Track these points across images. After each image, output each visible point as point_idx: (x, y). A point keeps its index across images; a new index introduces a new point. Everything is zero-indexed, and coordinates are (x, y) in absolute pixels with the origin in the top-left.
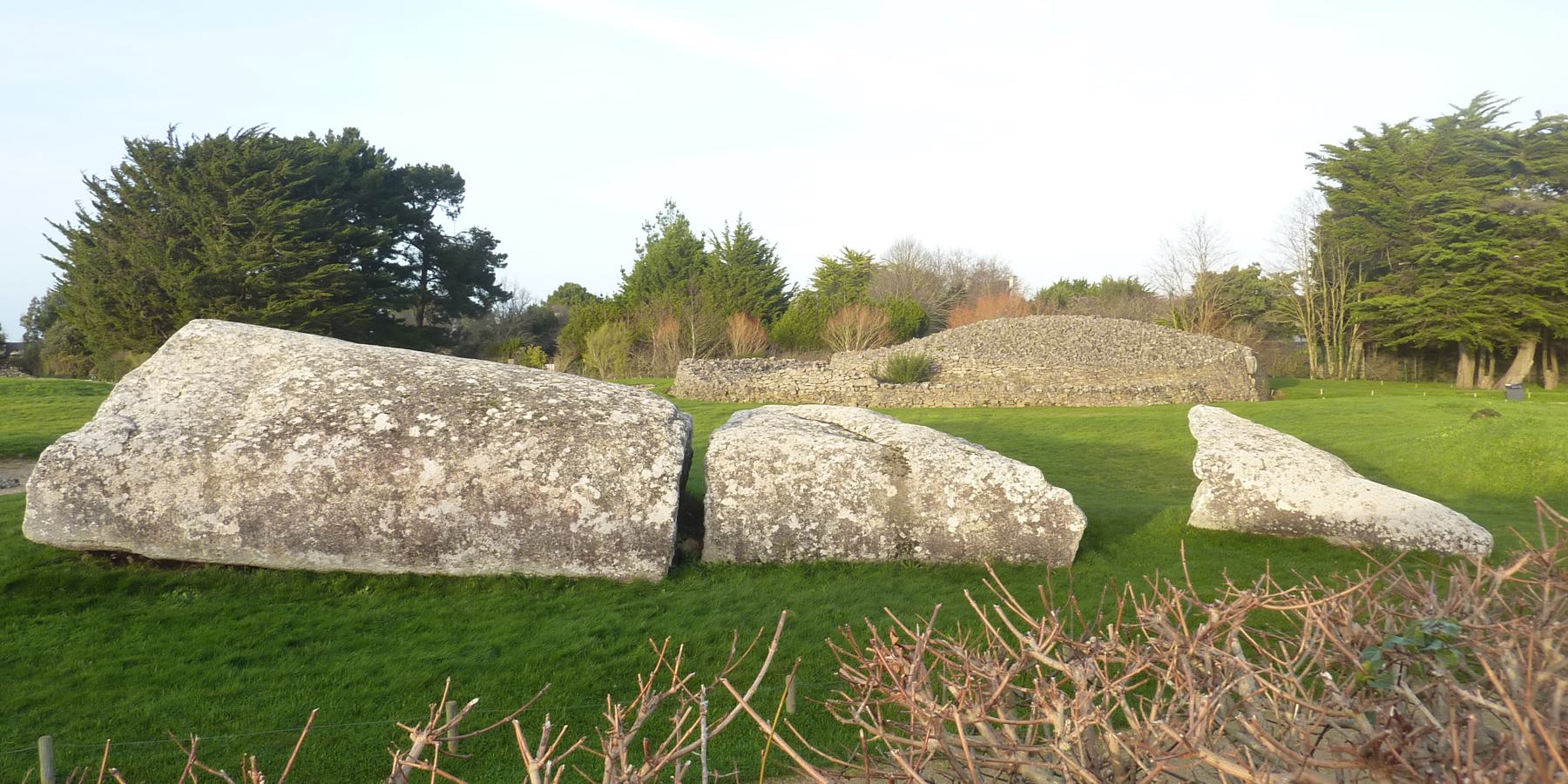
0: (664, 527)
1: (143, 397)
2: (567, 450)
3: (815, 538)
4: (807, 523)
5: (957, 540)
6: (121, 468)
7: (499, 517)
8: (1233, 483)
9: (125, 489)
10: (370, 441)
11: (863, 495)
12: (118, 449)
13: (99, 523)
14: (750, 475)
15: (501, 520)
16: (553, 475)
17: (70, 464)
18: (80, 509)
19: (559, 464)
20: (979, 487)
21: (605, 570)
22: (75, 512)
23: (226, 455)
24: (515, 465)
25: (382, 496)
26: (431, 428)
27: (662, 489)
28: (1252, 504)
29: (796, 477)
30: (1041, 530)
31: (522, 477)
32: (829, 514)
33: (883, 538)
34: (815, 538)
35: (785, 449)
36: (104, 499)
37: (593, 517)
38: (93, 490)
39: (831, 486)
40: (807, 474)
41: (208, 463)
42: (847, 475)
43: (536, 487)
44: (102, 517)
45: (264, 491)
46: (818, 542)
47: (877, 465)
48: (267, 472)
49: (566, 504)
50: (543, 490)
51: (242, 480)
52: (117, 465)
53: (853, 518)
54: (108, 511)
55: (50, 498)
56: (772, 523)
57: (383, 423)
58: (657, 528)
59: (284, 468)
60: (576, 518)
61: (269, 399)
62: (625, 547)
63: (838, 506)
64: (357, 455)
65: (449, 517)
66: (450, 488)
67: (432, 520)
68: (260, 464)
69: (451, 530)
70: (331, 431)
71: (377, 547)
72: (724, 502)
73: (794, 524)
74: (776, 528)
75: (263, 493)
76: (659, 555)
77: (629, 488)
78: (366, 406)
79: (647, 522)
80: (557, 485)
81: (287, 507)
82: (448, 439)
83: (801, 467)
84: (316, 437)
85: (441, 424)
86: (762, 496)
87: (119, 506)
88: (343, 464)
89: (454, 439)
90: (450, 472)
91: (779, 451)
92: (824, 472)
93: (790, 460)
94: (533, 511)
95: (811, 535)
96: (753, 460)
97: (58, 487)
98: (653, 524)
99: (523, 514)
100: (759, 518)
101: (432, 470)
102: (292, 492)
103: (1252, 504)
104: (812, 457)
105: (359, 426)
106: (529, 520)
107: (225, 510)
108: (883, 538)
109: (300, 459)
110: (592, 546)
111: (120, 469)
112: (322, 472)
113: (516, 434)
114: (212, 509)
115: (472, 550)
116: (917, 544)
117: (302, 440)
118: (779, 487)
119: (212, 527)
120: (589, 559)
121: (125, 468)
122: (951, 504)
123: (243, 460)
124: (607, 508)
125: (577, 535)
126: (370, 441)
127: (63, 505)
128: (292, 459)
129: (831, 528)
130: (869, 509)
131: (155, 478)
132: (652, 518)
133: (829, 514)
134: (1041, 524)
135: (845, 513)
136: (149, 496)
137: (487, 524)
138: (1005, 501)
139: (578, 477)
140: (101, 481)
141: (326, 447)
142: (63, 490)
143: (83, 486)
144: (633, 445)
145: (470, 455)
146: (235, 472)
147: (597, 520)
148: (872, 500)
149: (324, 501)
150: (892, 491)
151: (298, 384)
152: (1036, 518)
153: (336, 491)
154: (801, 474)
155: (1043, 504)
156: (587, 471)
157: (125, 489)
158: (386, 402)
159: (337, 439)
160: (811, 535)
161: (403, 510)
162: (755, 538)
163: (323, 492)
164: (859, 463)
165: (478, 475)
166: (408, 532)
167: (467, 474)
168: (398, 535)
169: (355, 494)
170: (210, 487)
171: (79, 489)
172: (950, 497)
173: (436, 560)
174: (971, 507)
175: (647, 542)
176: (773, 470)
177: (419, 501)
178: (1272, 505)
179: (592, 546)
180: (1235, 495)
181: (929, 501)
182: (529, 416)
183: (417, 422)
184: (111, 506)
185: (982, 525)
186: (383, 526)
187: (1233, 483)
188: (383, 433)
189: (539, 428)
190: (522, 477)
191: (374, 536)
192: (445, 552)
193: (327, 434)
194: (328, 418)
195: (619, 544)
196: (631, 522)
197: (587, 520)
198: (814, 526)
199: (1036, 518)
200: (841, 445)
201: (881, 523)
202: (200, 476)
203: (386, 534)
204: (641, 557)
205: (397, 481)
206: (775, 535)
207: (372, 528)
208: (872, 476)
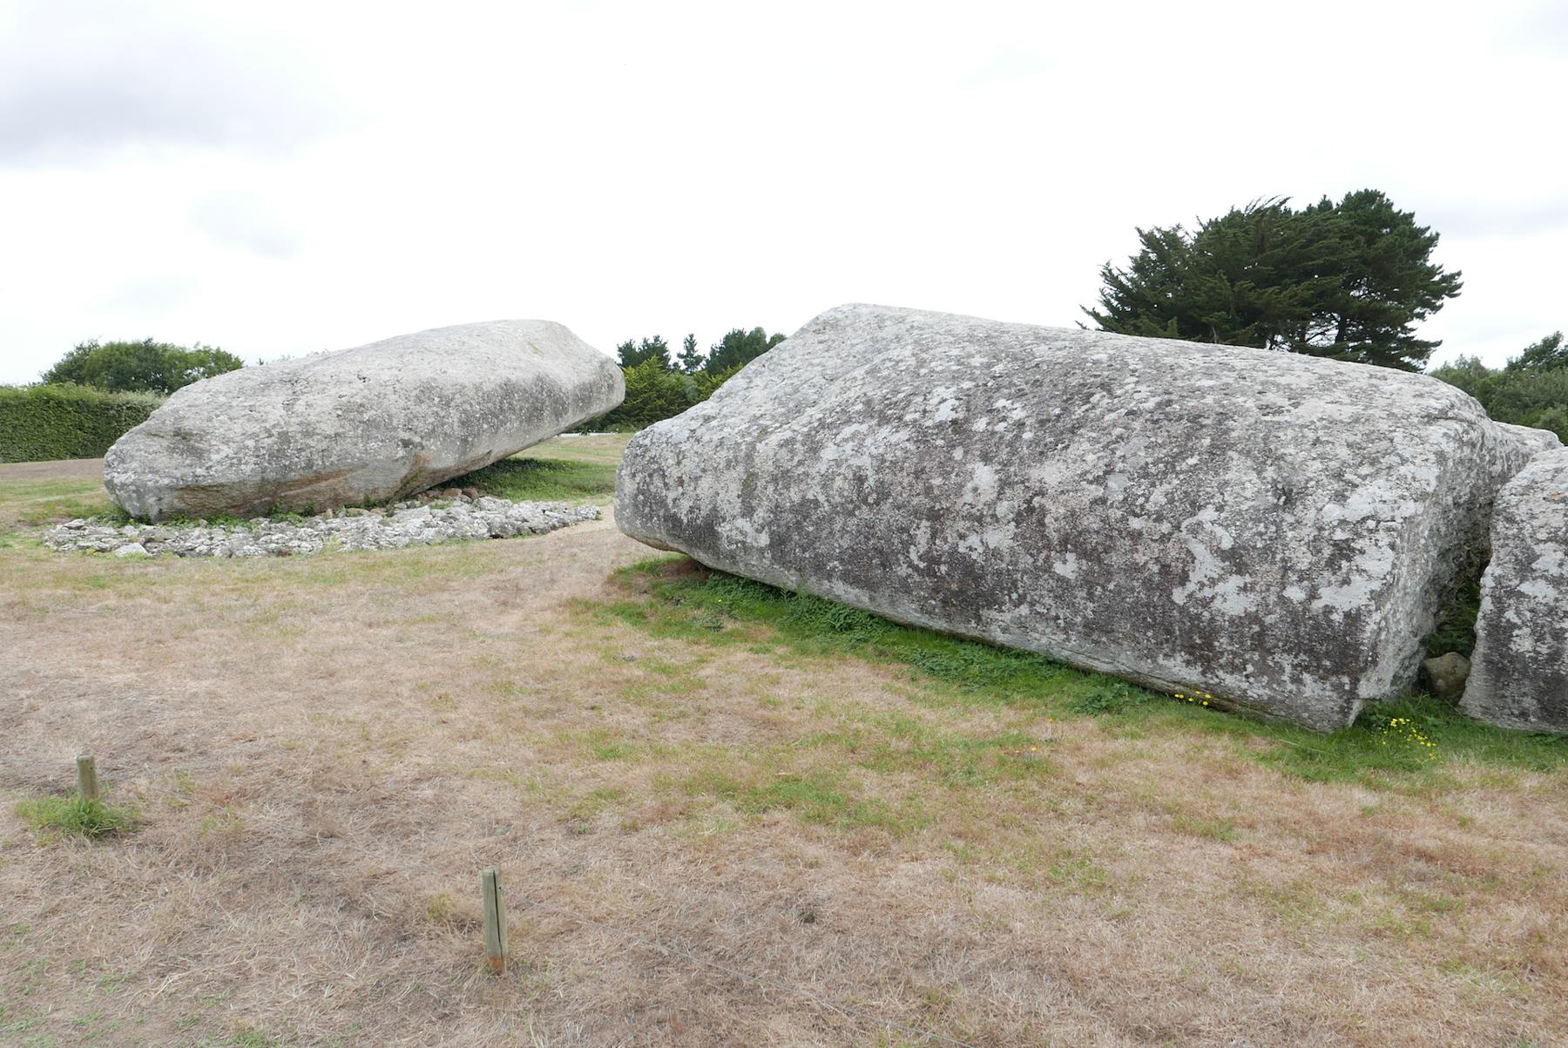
7: (1065, 562)
15: (1068, 567)
16: (1158, 497)
25: (917, 513)
27: (1358, 545)
38: (657, 481)
43: (1124, 519)
48: (801, 470)
50: (1135, 524)
51: (775, 480)
58: (1337, 617)
65: (996, 553)
71: (905, 587)
72: (1525, 588)
77: (1290, 534)
79: (1317, 605)
90: (1004, 484)
98: (1329, 610)
99: (1100, 561)
102: (822, 498)
114: (748, 512)
124: (1241, 569)
125: (1183, 609)
132: (1328, 596)
147: (1220, 588)
165: (1042, 493)
166: (943, 568)
191: (903, 570)
196: (1283, 601)
197: (1202, 585)
203: (916, 568)
207: (901, 558)
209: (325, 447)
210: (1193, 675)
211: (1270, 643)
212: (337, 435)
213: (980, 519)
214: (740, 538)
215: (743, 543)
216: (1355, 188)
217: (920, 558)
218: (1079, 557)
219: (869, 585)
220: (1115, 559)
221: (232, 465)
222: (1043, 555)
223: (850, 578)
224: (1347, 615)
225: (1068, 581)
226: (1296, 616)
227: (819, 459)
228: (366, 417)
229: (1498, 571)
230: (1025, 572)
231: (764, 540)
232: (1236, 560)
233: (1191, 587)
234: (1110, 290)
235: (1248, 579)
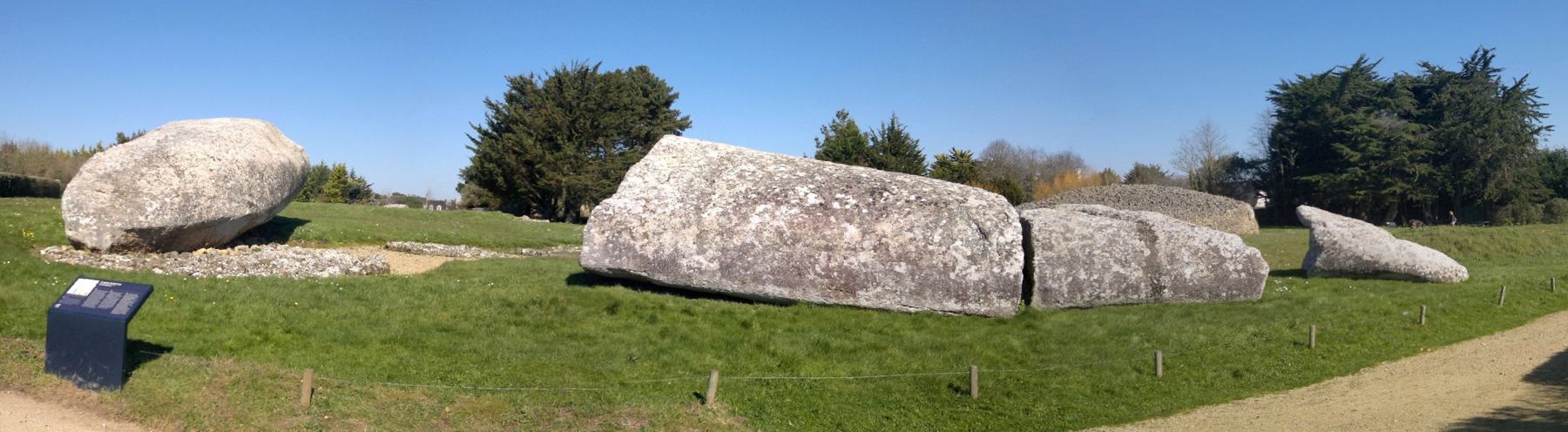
0: (1016, 276)
2: (944, 222)
3: (1097, 285)
4: (1091, 274)
5: (1191, 284)
6: (643, 221)
7: (900, 266)
8: (1337, 246)
9: (646, 235)
10: (807, 211)
11: (1128, 254)
12: (641, 210)
13: (628, 258)
14: (1050, 242)
15: (902, 268)
16: (937, 238)
17: (610, 220)
18: (612, 245)
19: (940, 231)
20: (1204, 248)
21: (973, 307)
22: (614, 249)
23: (711, 215)
24: (910, 230)
25: (818, 248)
26: (847, 203)
27: (1014, 250)
29: (1082, 243)
30: (1243, 275)
31: (915, 239)
32: (1106, 268)
33: (1143, 284)
34: (1097, 285)
35: (1071, 225)
36: (632, 242)
37: (965, 269)
38: (626, 236)
39: (1106, 249)
40: (1090, 242)
41: (699, 222)
43: (925, 246)
44: (630, 254)
45: (737, 241)
46: (1099, 288)
47: (1136, 235)
48: (738, 228)
49: (947, 258)
50: (930, 248)
51: (721, 234)
52: (641, 220)
53: (1122, 271)
54: (635, 250)
55: (599, 239)
56: (1067, 275)
57: (813, 199)
58: (1012, 277)
59: (749, 226)
60: (954, 271)
61: (731, 182)
62: (988, 290)
63: (1112, 263)
64: (800, 219)
65: (865, 265)
67: (853, 267)
68: (733, 224)
69: (866, 274)
70: (779, 203)
71: (813, 284)
73: (1083, 276)
74: (1070, 279)
75: (736, 242)
76: (1012, 296)
77: (990, 249)
78: (798, 188)
79: (1004, 274)
80: (941, 245)
81: (752, 253)
82: (860, 211)
83: (1084, 237)
84: (769, 206)
85: (854, 202)
87: (642, 246)
88: (791, 225)
89: (865, 211)
90: (864, 233)
91: (1068, 227)
92: (1101, 240)
93: (1076, 232)
95: (1094, 283)
96: (1051, 232)
97: (603, 232)
98: (1008, 274)
99: (917, 265)
100: (1059, 272)
101: (852, 231)
102: (756, 243)
104: (1091, 230)
105: (797, 201)
106: (921, 269)
107: (710, 253)
108: (1143, 284)
109: (761, 221)
110: (965, 291)
111: (643, 223)
112: (776, 230)
113: (907, 209)
114: (701, 252)
115: (879, 289)
116: (1165, 287)
117: (760, 208)
118: (1071, 250)
119: (701, 264)
120: (962, 297)
121: (646, 222)
122: (1186, 260)
123: (723, 220)
124: (975, 263)
125: (954, 281)
126: (807, 211)
127: (606, 244)
128: (755, 220)
129: (1108, 278)
131: (665, 229)
132: (1007, 270)
134: (1243, 270)
135: (1116, 268)
136: (661, 241)
137: (892, 270)
138: (1221, 256)
139: (954, 240)
140: (631, 230)
141: (777, 213)
142: (606, 235)
143: (619, 232)
144: (988, 220)
145: (879, 222)
146: (718, 228)
147: (968, 271)
150: (1147, 252)
151: (747, 174)
152: (1240, 267)
153: (785, 244)
154: (1085, 242)
155: (1244, 257)
156: (960, 236)
158: (812, 186)
159: (784, 208)
160: (1094, 283)
161: (832, 258)
162: (1055, 286)
163: (777, 244)
164: (1123, 233)
165: (885, 236)
166: (836, 274)
167: (877, 235)
168: (828, 277)
169: (799, 245)
170: (701, 237)
171: (616, 235)
172: (1185, 255)
173: (854, 296)
174: (1199, 261)
175: (1004, 288)
176: (1066, 239)
177: (843, 252)
178: (1360, 258)
180: (1339, 254)
181: (1172, 258)
182: (913, 198)
183: (837, 199)
184: (637, 247)
185: (1206, 273)
186: (818, 269)
187: (1337, 246)
188: (814, 205)
189: (922, 205)
190: (915, 239)
191: (811, 276)
192: (861, 289)
193: (776, 204)
194: (775, 195)
195: (984, 289)
196: (992, 273)
197: (962, 271)
198: (1096, 277)
200: (1109, 222)
201: (1140, 273)
202: (694, 230)
203: (819, 275)
204: (1000, 297)
205: (829, 238)
206: (1070, 284)
207: (810, 270)
208: (1133, 241)
209: (208, 205)
210: (958, 307)
211: (989, 289)
212: (215, 197)
213: (855, 249)
214: (696, 266)
215: (699, 269)
216: (639, 64)
217: (823, 270)
218: (907, 264)
219: (791, 286)
220: (924, 263)
221: (159, 215)
222: (889, 264)
223: (777, 283)
224: (1015, 276)
225: (902, 274)
226: (998, 278)
227: (749, 222)
228: (229, 185)
229: (1038, 258)
230: (880, 272)
231: (715, 265)
232: (972, 259)
233: (957, 271)
234: (491, 113)
235: (979, 266)
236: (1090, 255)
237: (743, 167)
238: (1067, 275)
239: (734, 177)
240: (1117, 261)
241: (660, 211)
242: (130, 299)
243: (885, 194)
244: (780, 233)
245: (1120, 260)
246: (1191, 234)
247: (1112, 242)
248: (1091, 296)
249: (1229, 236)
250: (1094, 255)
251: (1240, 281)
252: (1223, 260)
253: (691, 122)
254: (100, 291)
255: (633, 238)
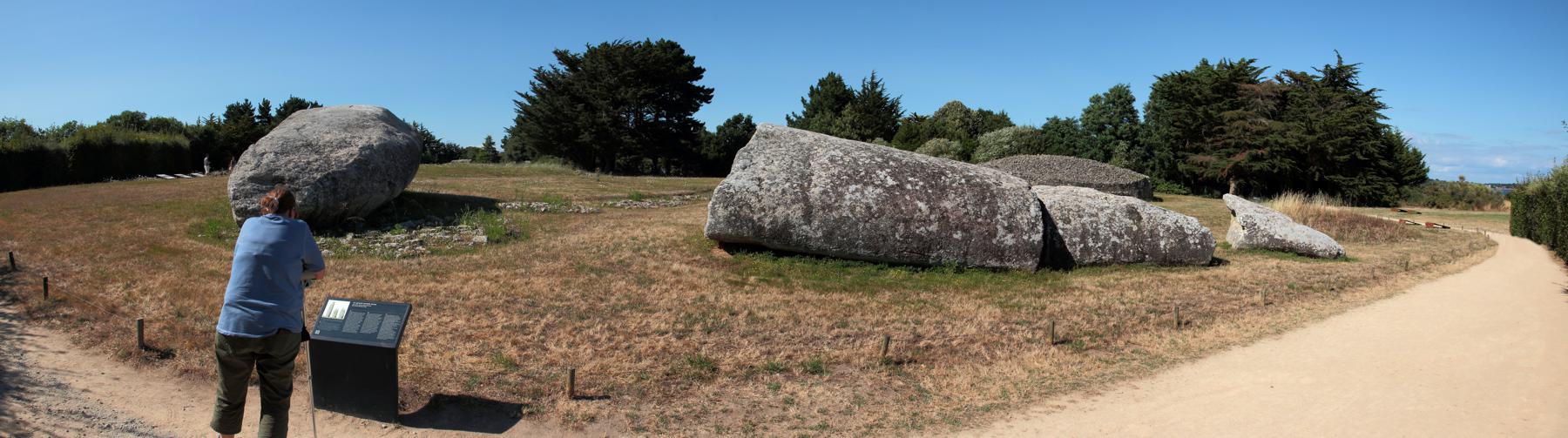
1: (754, 162)
22: (735, 221)
24: (964, 207)
28: (1264, 236)
30: (1199, 246)
32: (1107, 239)
42: (1114, 220)
48: (837, 204)
51: (823, 209)
53: (1118, 241)
56: (1080, 243)
58: (1036, 243)
63: (1111, 235)
66: (932, 217)
70: (866, 184)
74: (1082, 245)
82: (926, 191)
83: (1092, 215)
84: (859, 186)
86: (1075, 229)
87: (759, 219)
94: (974, 232)
97: (726, 207)
98: (1034, 241)
100: (1074, 240)
103: (1264, 236)
107: (816, 223)
110: (1003, 252)
118: (1083, 225)
124: (1011, 232)
130: (1125, 236)
133: (1107, 239)
134: (1199, 244)
135: (1114, 239)
148: (1126, 233)
149: (867, 222)
150: (1135, 228)
152: (1197, 241)
157: (763, 210)
158: (889, 170)
159: (870, 188)
164: (1118, 214)
179: (1003, 252)
188: (893, 186)
199: (1197, 241)
217: (901, 237)
236: (1097, 229)
237: (833, 153)
238: (1080, 243)
239: (827, 161)
240: (1115, 234)
241: (773, 189)
242: (391, 321)
243: (943, 178)
244: (869, 208)
245: (1117, 233)
246: (1164, 216)
247: (1111, 220)
248: (1096, 258)
249: (1190, 218)
250: (1099, 229)
251: (1196, 251)
252: (1186, 236)
253: (562, 56)
254: (355, 314)
255: (752, 211)
